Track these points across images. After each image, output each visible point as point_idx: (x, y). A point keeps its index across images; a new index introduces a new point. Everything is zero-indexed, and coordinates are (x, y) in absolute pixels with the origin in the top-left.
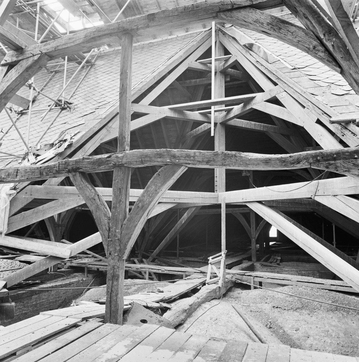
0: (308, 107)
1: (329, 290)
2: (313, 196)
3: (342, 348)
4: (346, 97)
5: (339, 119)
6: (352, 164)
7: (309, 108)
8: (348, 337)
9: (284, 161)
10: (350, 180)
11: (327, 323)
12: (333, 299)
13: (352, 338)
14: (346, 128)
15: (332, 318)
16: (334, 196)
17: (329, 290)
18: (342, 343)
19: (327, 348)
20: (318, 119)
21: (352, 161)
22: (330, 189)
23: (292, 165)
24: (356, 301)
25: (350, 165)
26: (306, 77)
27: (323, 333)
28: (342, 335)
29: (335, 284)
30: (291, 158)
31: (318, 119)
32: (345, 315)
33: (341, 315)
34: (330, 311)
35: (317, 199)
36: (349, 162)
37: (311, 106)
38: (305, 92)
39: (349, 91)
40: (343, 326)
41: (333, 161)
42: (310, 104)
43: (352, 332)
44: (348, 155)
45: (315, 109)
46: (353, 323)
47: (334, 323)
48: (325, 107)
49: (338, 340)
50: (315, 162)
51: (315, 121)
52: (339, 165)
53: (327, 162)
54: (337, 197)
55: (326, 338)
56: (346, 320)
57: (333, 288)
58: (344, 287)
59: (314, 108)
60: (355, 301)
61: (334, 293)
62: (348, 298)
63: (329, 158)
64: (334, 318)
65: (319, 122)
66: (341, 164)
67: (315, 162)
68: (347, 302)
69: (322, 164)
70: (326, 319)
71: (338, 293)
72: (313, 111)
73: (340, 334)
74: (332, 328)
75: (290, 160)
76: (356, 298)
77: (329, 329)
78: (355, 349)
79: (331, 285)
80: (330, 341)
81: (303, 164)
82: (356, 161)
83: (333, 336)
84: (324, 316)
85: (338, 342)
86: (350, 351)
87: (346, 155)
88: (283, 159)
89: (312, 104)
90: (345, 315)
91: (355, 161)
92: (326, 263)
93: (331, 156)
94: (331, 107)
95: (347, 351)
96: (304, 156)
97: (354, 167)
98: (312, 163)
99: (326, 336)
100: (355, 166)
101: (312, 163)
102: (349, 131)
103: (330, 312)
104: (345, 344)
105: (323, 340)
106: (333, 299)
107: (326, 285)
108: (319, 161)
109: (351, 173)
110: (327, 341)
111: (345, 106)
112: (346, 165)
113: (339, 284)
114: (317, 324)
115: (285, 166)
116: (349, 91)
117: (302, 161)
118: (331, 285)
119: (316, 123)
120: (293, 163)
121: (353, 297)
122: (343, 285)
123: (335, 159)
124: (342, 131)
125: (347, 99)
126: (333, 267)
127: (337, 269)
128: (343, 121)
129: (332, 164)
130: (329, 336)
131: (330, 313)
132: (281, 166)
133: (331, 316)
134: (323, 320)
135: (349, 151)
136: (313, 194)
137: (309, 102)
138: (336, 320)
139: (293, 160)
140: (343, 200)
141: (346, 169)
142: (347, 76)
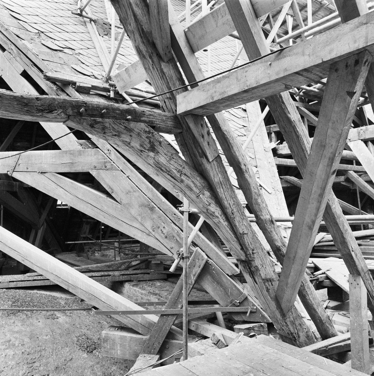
0: (10, 51)
1: (7, 288)
2: (11, 172)
3: (28, 356)
4: (60, 54)
5: (57, 77)
6: (123, 127)
7: (12, 52)
8: (35, 341)
9: (26, 105)
10: (64, 155)
11: (8, 331)
12: (12, 298)
13: (38, 340)
14: (63, 91)
15: (14, 323)
16: (42, 173)
17: (7, 288)
18: (28, 350)
19: (10, 362)
20: (24, 70)
21: (123, 123)
22: (36, 164)
23: (40, 114)
24: (38, 295)
25: (121, 128)
26: (6, 11)
27: (4, 345)
28: (27, 340)
29: (15, 280)
30: (38, 102)
31: (24, 70)
32: (30, 315)
33: (25, 316)
34: (11, 315)
35: (16, 175)
36: (120, 124)
37: (15, 51)
38: (7, 30)
39: (63, 48)
40: (28, 329)
41: (101, 119)
42: (13, 47)
43: (38, 333)
44: (119, 114)
45: (21, 56)
46: (39, 322)
47: (16, 329)
48: (36, 57)
49: (23, 348)
50: (75, 114)
51: (20, 73)
52: (107, 125)
53: (92, 118)
54: (46, 175)
55: (8, 350)
56: (31, 321)
57: (12, 285)
58: (25, 282)
59: (20, 54)
60: (38, 295)
61: (13, 290)
62: (30, 293)
63: (94, 114)
64: (16, 322)
65: (25, 75)
66: (110, 124)
67: (75, 114)
68: (30, 299)
69: (85, 119)
70: (6, 326)
71: (18, 290)
72: (18, 59)
73: (25, 340)
74: (15, 335)
75: (36, 104)
76: (38, 292)
77: (11, 338)
78: (43, 352)
79: (10, 282)
80: (13, 353)
81: (58, 115)
82: (128, 123)
83: (17, 345)
84: (4, 322)
85: (23, 351)
86: (37, 357)
87: (117, 113)
88: (25, 101)
89: (17, 49)
90: (30, 315)
91: (127, 124)
92: (23, 259)
93: (97, 110)
94: (43, 60)
95: (34, 358)
96: (59, 103)
97: (125, 131)
98: (71, 116)
99: (7, 349)
100: (127, 130)
101: (71, 116)
102: (66, 94)
103: (12, 316)
104: (32, 349)
105: (4, 355)
106: (12, 298)
107: (3, 283)
108: (81, 114)
109: (121, 138)
110: (9, 354)
111: (59, 65)
112: (116, 127)
113: (20, 280)
114: (40, 351)
115: (28, 113)
116: (63, 48)
117: (56, 110)
118: (10, 282)
119: (21, 74)
120: (42, 111)
121: (35, 291)
122: (25, 280)
123: (102, 116)
124: (57, 93)
125: (61, 56)
126: (34, 262)
127: (38, 265)
128: (62, 80)
129: (99, 122)
130: (11, 347)
131: (11, 317)
132: (20, 112)
133: (12, 321)
134: (3, 328)
135: (121, 108)
136: (10, 169)
137: (12, 45)
138: (19, 324)
139: (42, 105)
140: (53, 179)
141: (116, 132)
142: (122, 6)
